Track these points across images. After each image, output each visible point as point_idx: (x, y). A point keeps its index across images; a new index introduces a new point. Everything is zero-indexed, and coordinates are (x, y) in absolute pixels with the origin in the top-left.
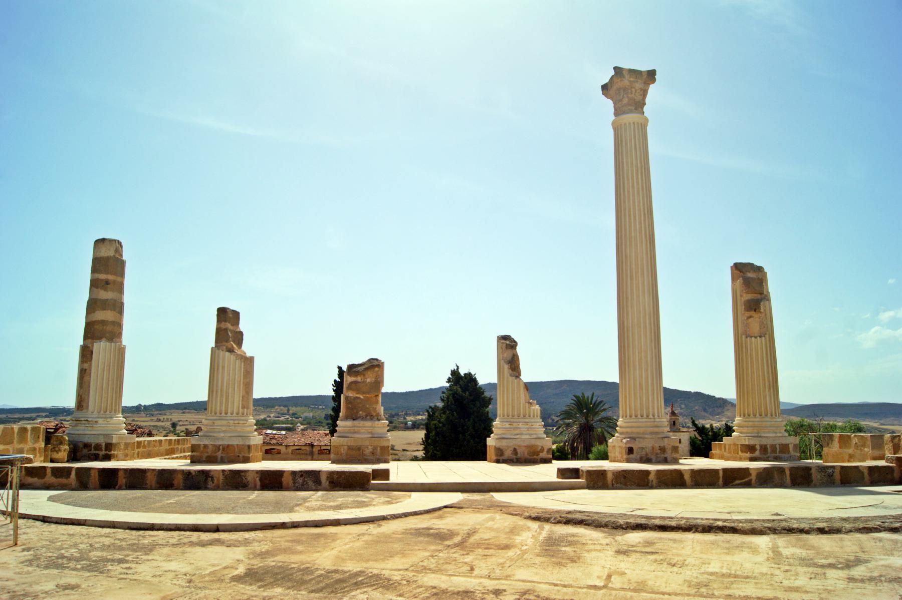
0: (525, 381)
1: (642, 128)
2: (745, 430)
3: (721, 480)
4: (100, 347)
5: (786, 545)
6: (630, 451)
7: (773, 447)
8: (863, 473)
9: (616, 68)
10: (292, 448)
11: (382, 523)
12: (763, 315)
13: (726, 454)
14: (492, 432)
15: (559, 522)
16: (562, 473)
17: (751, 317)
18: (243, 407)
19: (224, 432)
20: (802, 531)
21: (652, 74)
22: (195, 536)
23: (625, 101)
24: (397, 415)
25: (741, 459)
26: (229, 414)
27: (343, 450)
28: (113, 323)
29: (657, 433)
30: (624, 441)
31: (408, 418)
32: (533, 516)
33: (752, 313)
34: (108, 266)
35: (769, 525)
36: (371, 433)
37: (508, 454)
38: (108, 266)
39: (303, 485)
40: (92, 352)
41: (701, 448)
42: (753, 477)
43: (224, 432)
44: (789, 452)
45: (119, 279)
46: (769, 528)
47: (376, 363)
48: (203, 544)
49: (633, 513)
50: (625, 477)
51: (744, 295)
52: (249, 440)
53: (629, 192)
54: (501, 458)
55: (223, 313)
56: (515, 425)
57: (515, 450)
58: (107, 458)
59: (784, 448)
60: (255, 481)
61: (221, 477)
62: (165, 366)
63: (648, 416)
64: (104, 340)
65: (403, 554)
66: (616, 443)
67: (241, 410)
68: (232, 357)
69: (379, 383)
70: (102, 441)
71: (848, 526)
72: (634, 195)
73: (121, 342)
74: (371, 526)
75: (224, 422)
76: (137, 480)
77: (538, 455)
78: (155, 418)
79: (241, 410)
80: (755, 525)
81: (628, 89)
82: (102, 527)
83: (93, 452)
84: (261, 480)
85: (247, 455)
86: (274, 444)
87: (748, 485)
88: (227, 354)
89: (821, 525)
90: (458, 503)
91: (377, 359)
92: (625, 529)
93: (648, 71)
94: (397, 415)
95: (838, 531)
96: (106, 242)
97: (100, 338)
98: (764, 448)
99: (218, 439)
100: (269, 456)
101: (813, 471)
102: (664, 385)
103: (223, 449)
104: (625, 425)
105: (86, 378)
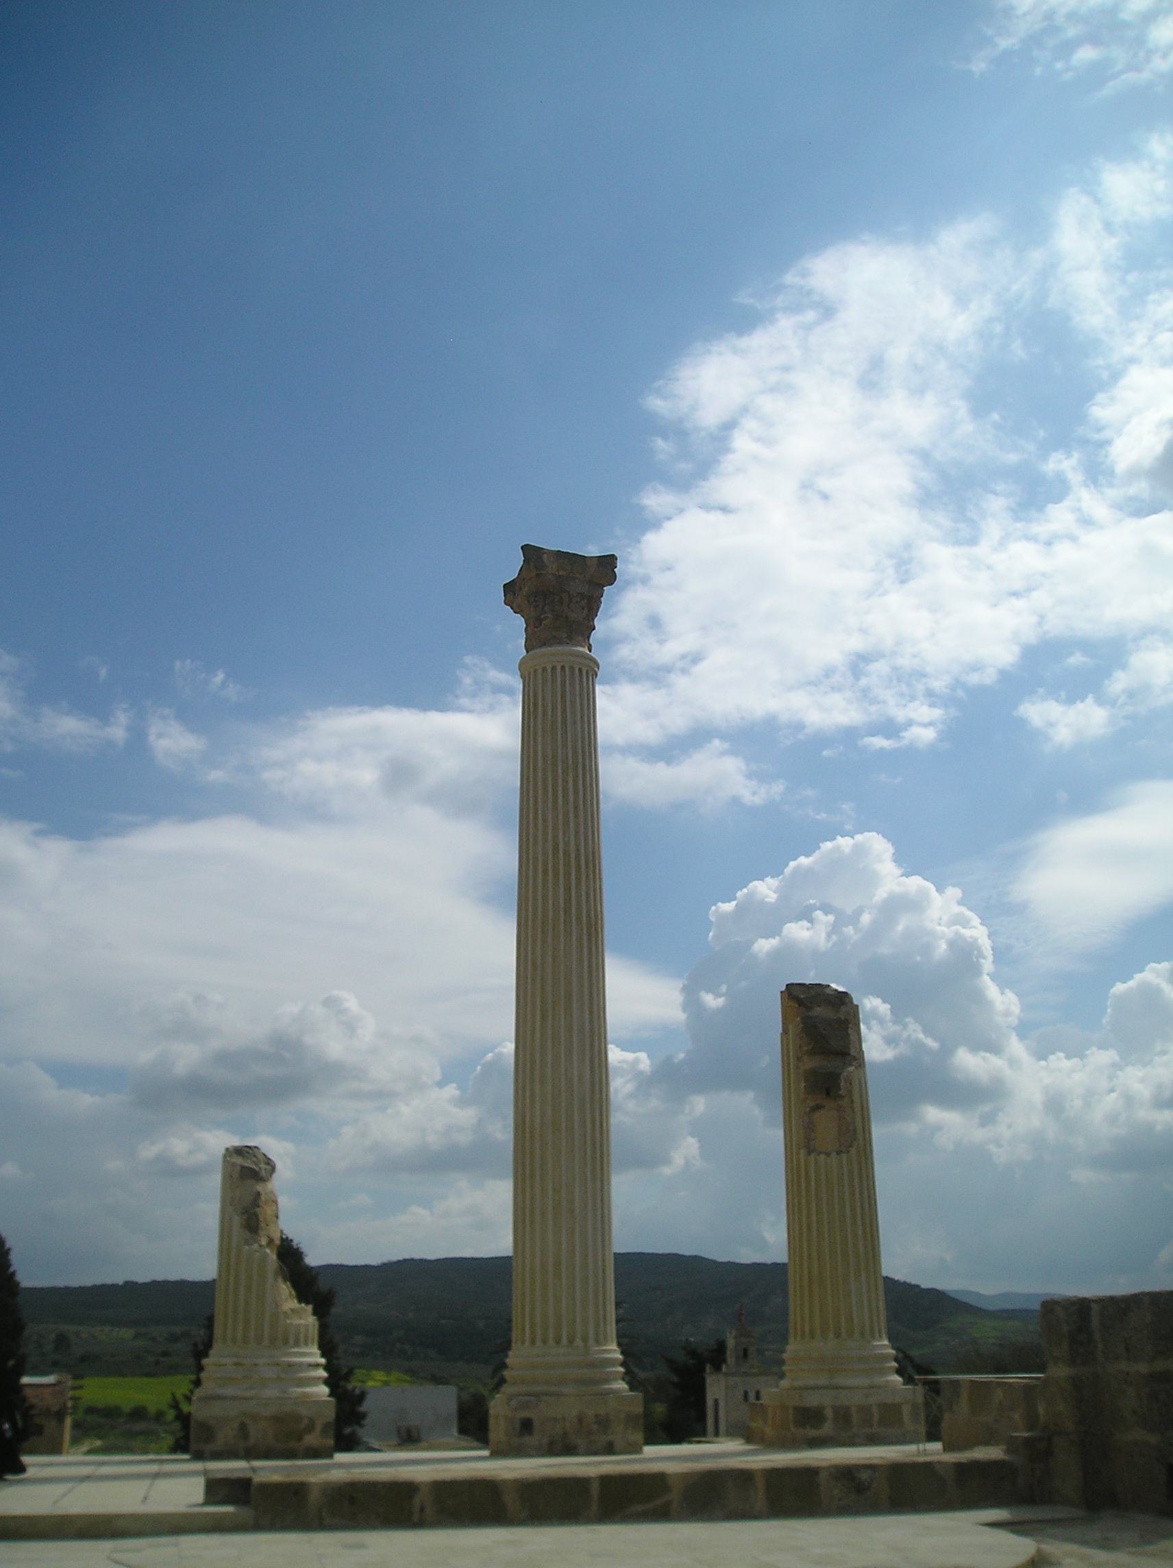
7: (865, 1410)
9: (526, 549)
13: (769, 1431)
16: (217, 1489)
41: (682, 1418)
50: (352, 1500)
57: (243, 1427)
72: (555, 828)
77: (300, 1439)
87: (663, 1514)
101: (823, 1476)
102: (886, 1272)
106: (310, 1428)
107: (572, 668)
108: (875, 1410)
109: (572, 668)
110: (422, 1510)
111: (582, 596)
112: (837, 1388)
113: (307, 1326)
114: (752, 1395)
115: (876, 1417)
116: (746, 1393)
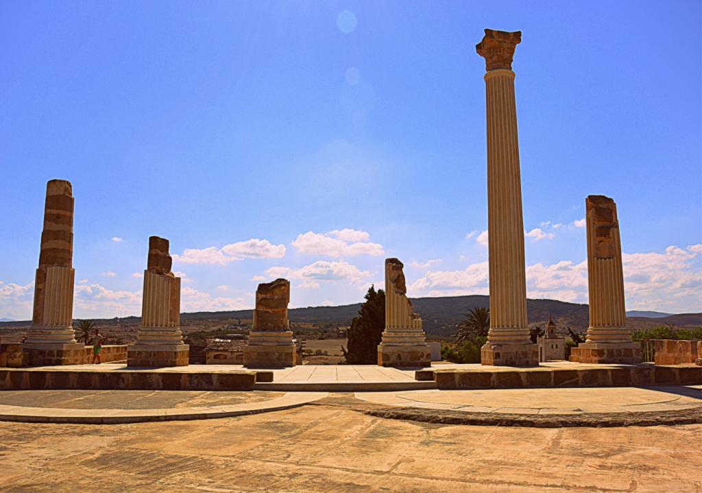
0: (408, 297)
1: (510, 81)
2: (596, 337)
3: (552, 380)
4: (52, 271)
5: (568, 437)
6: (497, 355)
8: (674, 374)
9: (486, 30)
10: (236, 354)
11: (243, 417)
12: (612, 240)
14: (381, 341)
15: (391, 417)
16: (418, 376)
17: (601, 241)
18: (171, 321)
19: (155, 341)
20: (588, 425)
21: (518, 34)
22: (88, 427)
23: (495, 58)
24: (331, 325)
25: (591, 362)
26: (159, 326)
27: (254, 356)
28: (63, 250)
29: (520, 341)
30: (492, 347)
31: (340, 329)
32: (372, 412)
33: (602, 238)
34: (59, 203)
35: (563, 420)
36: (278, 342)
37: (393, 359)
38: (59, 203)
39: (197, 385)
40: (46, 274)
42: (580, 378)
43: (155, 341)
44: (632, 356)
45: (68, 213)
46: (562, 422)
47: (283, 282)
48: (81, 434)
49: (460, 409)
51: (596, 223)
52: (176, 348)
53: (498, 136)
54: (387, 362)
55: (154, 241)
56: (399, 334)
58: (59, 363)
59: (628, 352)
60: (158, 381)
61: (131, 379)
62: (108, 288)
63: (513, 326)
64: (56, 264)
65: (240, 444)
66: (487, 349)
67: (169, 323)
68: (161, 278)
69: (285, 299)
70: (54, 348)
71: (629, 420)
72: (502, 138)
73: (71, 266)
74: (232, 419)
75: (155, 333)
76: (86, 382)
77: (419, 359)
78: (129, 330)
79: (169, 323)
80: (550, 420)
81: (498, 48)
82: (6, 421)
83: (47, 358)
84: (162, 381)
85: (174, 360)
86: (221, 351)
88: (157, 275)
89: (606, 419)
90: (319, 401)
91: (283, 280)
92: (444, 423)
93: (515, 33)
94: (331, 325)
95: (620, 424)
96: (57, 183)
97: (52, 263)
98: (611, 353)
99: (150, 346)
100: (217, 361)
103: (154, 355)
104: (493, 334)
105: (41, 297)
106: (422, 356)
107: (506, 77)
108: (622, 351)
109: (506, 77)
110: (494, 382)
111: (509, 48)
112: (609, 343)
113: (419, 321)
114: (555, 346)
115: (623, 353)
116: (552, 345)
